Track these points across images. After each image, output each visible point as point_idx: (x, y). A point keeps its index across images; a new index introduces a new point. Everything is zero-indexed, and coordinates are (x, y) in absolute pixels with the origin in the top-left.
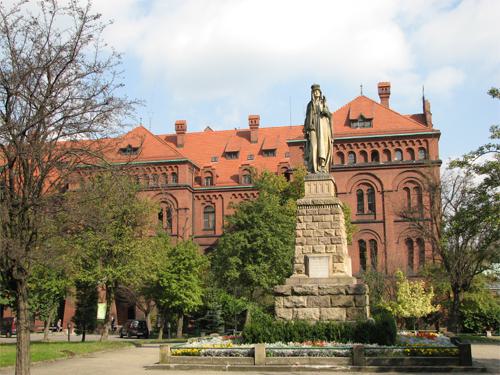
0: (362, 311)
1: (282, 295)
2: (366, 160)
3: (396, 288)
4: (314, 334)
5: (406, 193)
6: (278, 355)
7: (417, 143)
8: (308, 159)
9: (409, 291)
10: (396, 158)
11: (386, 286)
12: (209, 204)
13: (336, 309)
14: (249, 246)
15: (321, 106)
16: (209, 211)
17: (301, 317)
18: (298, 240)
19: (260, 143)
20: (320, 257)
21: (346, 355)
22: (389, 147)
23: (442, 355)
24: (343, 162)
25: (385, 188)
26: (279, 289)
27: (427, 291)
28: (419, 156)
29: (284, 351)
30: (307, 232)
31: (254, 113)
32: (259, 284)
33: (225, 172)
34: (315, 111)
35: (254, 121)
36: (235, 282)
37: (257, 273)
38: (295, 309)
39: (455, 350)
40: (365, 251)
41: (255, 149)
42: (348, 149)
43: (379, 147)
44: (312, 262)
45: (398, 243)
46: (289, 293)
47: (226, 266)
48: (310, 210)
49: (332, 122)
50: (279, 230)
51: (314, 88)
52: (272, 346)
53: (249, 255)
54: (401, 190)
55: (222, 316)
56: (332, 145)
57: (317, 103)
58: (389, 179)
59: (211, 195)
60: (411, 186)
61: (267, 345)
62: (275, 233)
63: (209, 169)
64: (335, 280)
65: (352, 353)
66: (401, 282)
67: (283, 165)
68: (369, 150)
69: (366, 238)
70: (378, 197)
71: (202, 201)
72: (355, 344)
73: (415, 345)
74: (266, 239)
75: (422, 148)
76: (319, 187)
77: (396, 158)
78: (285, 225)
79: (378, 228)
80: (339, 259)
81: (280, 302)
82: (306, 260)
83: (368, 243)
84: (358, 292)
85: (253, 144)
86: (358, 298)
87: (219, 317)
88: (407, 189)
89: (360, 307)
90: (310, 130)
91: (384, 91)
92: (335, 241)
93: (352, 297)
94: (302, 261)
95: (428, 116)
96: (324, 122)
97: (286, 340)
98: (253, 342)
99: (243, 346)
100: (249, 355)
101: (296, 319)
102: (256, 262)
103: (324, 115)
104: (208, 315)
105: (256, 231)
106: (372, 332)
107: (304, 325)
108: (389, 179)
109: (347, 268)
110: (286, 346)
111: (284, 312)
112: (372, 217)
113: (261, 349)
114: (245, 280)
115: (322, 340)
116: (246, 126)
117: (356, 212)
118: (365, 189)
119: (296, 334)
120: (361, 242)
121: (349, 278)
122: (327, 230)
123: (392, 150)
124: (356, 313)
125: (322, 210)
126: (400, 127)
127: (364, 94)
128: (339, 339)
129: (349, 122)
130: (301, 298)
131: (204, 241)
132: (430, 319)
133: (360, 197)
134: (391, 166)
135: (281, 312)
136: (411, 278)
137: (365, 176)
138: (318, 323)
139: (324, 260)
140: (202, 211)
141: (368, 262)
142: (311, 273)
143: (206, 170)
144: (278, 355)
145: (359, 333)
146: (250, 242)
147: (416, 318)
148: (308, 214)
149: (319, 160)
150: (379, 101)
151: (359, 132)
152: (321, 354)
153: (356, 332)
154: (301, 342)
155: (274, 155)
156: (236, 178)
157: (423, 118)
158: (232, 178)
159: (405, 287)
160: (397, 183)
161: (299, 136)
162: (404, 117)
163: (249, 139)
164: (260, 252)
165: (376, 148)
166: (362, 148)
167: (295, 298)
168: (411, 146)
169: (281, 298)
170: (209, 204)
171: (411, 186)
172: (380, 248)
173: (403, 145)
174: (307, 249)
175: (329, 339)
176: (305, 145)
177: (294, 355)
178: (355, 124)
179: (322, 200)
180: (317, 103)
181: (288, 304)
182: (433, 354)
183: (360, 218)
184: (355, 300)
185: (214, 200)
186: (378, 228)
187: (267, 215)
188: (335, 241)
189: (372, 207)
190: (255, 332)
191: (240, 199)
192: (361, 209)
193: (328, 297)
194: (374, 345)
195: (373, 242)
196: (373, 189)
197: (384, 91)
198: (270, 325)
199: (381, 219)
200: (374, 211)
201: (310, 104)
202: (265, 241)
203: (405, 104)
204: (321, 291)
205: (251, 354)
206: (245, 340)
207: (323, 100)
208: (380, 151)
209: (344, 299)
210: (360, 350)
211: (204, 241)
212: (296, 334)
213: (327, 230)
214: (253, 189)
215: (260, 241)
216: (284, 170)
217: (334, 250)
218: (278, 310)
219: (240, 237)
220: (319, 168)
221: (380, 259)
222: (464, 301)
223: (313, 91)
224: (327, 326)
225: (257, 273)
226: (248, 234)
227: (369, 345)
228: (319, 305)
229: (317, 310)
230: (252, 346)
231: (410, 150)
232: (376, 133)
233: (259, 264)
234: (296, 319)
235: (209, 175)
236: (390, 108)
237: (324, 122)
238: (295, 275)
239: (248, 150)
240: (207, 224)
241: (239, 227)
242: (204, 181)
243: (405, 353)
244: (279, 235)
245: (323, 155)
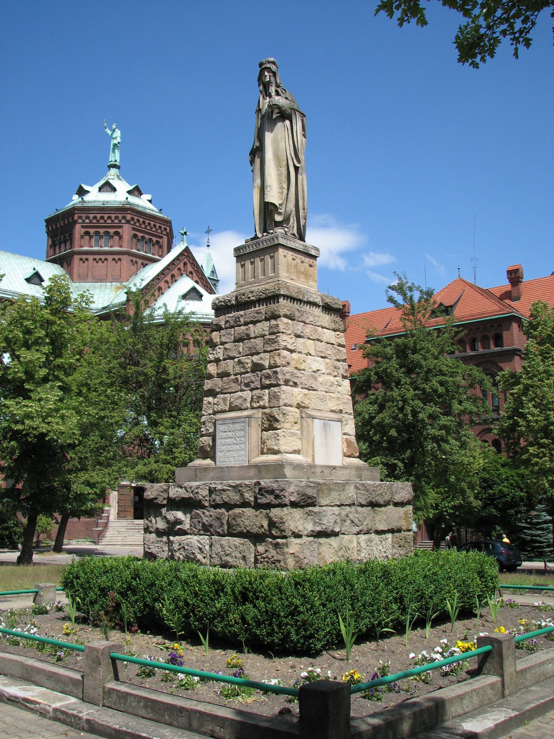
228: (206, 529)
229: (205, 539)
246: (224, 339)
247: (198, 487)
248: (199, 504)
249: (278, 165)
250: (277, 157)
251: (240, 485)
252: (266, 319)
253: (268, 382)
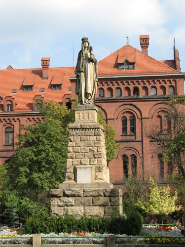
0: (116, 210)
1: (56, 196)
2: (129, 94)
3: (149, 192)
4: (79, 226)
5: (159, 120)
6: (50, 242)
7: (168, 82)
8: (78, 93)
9: (158, 194)
10: (152, 93)
11: (140, 191)
12: (9, 125)
13: (97, 207)
14: (35, 158)
15: (89, 54)
16: (9, 131)
17: (70, 213)
18: (69, 155)
19: (50, 79)
20: (85, 168)
21: (102, 243)
22: (147, 85)
23: (173, 243)
24: (112, 95)
25: (108, 117)
26: (54, 192)
27: (172, 195)
28: (169, 91)
29: (55, 239)
30: (76, 149)
31: (46, 56)
32: (42, 188)
33: (22, 101)
34: (84, 58)
35: (45, 62)
36: (25, 186)
37: (41, 179)
38: (66, 207)
39: (183, 239)
40: (129, 163)
41: (46, 83)
42: (116, 86)
43: (139, 84)
44: (79, 172)
45: (152, 157)
46: (61, 195)
47: (18, 174)
48: (78, 132)
49: (97, 67)
50: (59, 147)
51: (84, 40)
52: (46, 235)
53: (35, 166)
54: (155, 118)
55: (17, 212)
56: (96, 84)
57: (86, 51)
58: (147, 109)
59: (11, 118)
60: (163, 115)
61: (43, 235)
62: (56, 149)
63: (10, 99)
64: (96, 186)
65: (106, 241)
66: (153, 187)
67: (67, 97)
68: (131, 87)
69: (129, 153)
70: (137, 121)
71: (4, 123)
72: (110, 234)
73: (154, 235)
74: (49, 152)
75: (171, 86)
76: (86, 114)
77: (152, 93)
78: (63, 143)
79: (137, 146)
80: (99, 169)
81: (54, 202)
82: (75, 170)
83: (129, 157)
84: (113, 194)
85: (44, 80)
86: (113, 199)
87: (14, 214)
88: (159, 117)
89: (115, 206)
90: (80, 72)
91: (145, 42)
92: (97, 156)
93: (108, 198)
94: (72, 171)
95: (177, 62)
96: (90, 66)
97: (58, 232)
98: (33, 233)
99: (25, 236)
100: (28, 243)
101: (66, 215)
102: (40, 171)
103: (91, 60)
104: (6, 212)
105: (41, 147)
106: (124, 224)
107: (72, 220)
108: (147, 109)
109: (106, 176)
110: (57, 236)
111: (57, 209)
112: (133, 138)
113: (37, 238)
114: (32, 185)
115: (85, 231)
116: (39, 66)
117: (121, 133)
118: (128, 116)
119: (66, 226)
120: (124, 156)
121: (106, 184)
122: (91, 148)
123: (149, 87)
124: (111, 211)
125: (88, 132)
126: (155, 69)
127: (130, 44)
128: (98, 231)
129: (117, 65)
130: (70, 199)
131: (5, 154)
132: (174, 216)
133: (124, 122)
134: (147, 99)
135: (56, 210)
136: (162, 184)
137: (129, 107)
138: (82, 218)
139: (88, 171)
140: (4, 131)
141: (130, 172)
142: (78, 179)
143: (8, 99)
144: (50, 242)
145: (113, 226)
146: (36, 156)
147: (164, 215)
148: (77, 135)
149: (87, 94)
150: (140, 49)
151: (124, 72)
152: (83, 242)
153: (111, 225)
154: (69, 232)
155: (60, 89)
156: (31, 106)
157: (173, 64)
158: (27, 105)
159: (156, 191)
160: (152, 112)
161: (74, 77)
162: (159, 62)
163: (41, 76)
164: (44, 164)
165: (137, 85)
166: (126, 85)
167: (66, 199)
168: (163, 84)
169: (56, 199)
170: (9, 125)
171: (163, 115)
172: (139, 161)
173: (157, 83)
174: (76, 162)
175: (91, 231)
176: (77, 81)
177: (63, 243)
178: (122, 67)
179: (88, 125)
180: (86, 51)
181: (60, 204)
182: (166, 243)
183: (124, 138)
184: (110, 201)
185: (13, 123)
186: (137, 146)
187: (50, 135)
188: (97, 156)
189: (133, 130)
190: (35, 225)
191: (33, 122)
192: (124, 129)
193: (91, 198)
194: (124, 235)
195: (134, 157)
196: (134, 116)
197: (144, 42)
198: (46, 219)
199: (140, 139)
200: (135, 133)
201: (81, 53)
202: (47, 155)
203: (160, 52)
204: (85, 194)
205: (30, 242)
206: (27, 232)
207: (91, 49)
208: (140, 87)
209: (102, 200)
210: (112, 239)
211: (5, 154)
212: (66, 226)
213: (91, 148)
214: (38, 115)
215: (43, 155)
216: (67, 101)
217: (96, 163)
218: (53, 208)
219: (29, 152)
220: (87, 101)
221: (139, 170)
222: (119, 198)
223: (83, 43)
224: (89, 220)
225: (41, 179)
226: (35, 150)
227: (120, 235)
228: (84, 204)
230: (31, 236)
231: (163, 88)
232: (137, 74)
233: (42, 172)
234: (66, 215)
235: (11, 103)
236: (149, 55)
237: (90, 66)
238: (67, 181)
239: (41, 85)
240: (7, 141)
241: (28, 144)
242: (6, 108)
243: (146, 241)
244: (59, 150)
245: (90, 91)
246: (75, 140)
247: (79, 190)
248: (79, 196)
249: (91, 80)
250: (91, 78)
251: (98, 190)
252: (94, 135)
253: (97, 157)
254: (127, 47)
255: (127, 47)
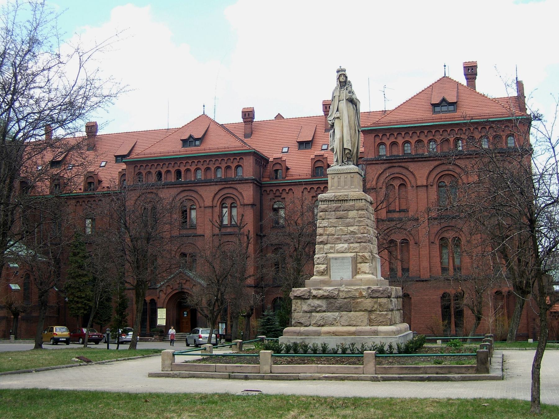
91: (471, 71)
251: (359, 289)
254: (445, 80)
255: (445, 80)
